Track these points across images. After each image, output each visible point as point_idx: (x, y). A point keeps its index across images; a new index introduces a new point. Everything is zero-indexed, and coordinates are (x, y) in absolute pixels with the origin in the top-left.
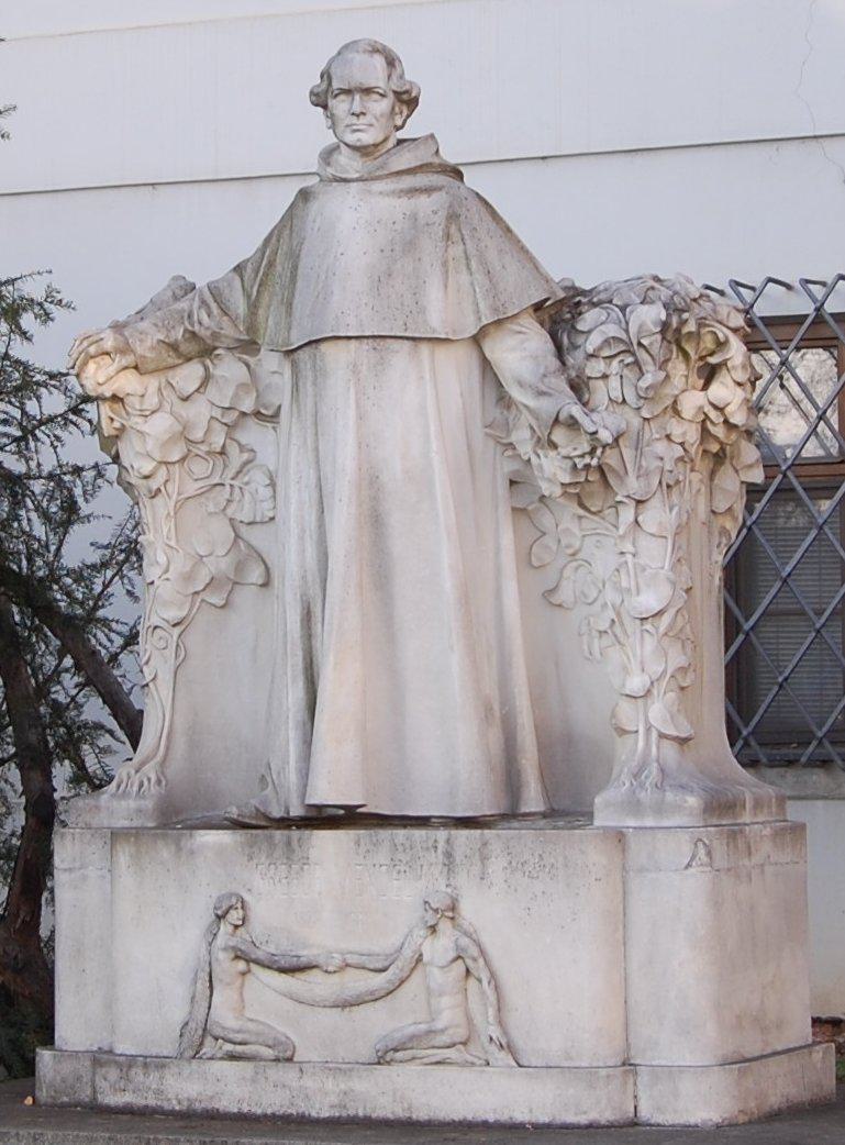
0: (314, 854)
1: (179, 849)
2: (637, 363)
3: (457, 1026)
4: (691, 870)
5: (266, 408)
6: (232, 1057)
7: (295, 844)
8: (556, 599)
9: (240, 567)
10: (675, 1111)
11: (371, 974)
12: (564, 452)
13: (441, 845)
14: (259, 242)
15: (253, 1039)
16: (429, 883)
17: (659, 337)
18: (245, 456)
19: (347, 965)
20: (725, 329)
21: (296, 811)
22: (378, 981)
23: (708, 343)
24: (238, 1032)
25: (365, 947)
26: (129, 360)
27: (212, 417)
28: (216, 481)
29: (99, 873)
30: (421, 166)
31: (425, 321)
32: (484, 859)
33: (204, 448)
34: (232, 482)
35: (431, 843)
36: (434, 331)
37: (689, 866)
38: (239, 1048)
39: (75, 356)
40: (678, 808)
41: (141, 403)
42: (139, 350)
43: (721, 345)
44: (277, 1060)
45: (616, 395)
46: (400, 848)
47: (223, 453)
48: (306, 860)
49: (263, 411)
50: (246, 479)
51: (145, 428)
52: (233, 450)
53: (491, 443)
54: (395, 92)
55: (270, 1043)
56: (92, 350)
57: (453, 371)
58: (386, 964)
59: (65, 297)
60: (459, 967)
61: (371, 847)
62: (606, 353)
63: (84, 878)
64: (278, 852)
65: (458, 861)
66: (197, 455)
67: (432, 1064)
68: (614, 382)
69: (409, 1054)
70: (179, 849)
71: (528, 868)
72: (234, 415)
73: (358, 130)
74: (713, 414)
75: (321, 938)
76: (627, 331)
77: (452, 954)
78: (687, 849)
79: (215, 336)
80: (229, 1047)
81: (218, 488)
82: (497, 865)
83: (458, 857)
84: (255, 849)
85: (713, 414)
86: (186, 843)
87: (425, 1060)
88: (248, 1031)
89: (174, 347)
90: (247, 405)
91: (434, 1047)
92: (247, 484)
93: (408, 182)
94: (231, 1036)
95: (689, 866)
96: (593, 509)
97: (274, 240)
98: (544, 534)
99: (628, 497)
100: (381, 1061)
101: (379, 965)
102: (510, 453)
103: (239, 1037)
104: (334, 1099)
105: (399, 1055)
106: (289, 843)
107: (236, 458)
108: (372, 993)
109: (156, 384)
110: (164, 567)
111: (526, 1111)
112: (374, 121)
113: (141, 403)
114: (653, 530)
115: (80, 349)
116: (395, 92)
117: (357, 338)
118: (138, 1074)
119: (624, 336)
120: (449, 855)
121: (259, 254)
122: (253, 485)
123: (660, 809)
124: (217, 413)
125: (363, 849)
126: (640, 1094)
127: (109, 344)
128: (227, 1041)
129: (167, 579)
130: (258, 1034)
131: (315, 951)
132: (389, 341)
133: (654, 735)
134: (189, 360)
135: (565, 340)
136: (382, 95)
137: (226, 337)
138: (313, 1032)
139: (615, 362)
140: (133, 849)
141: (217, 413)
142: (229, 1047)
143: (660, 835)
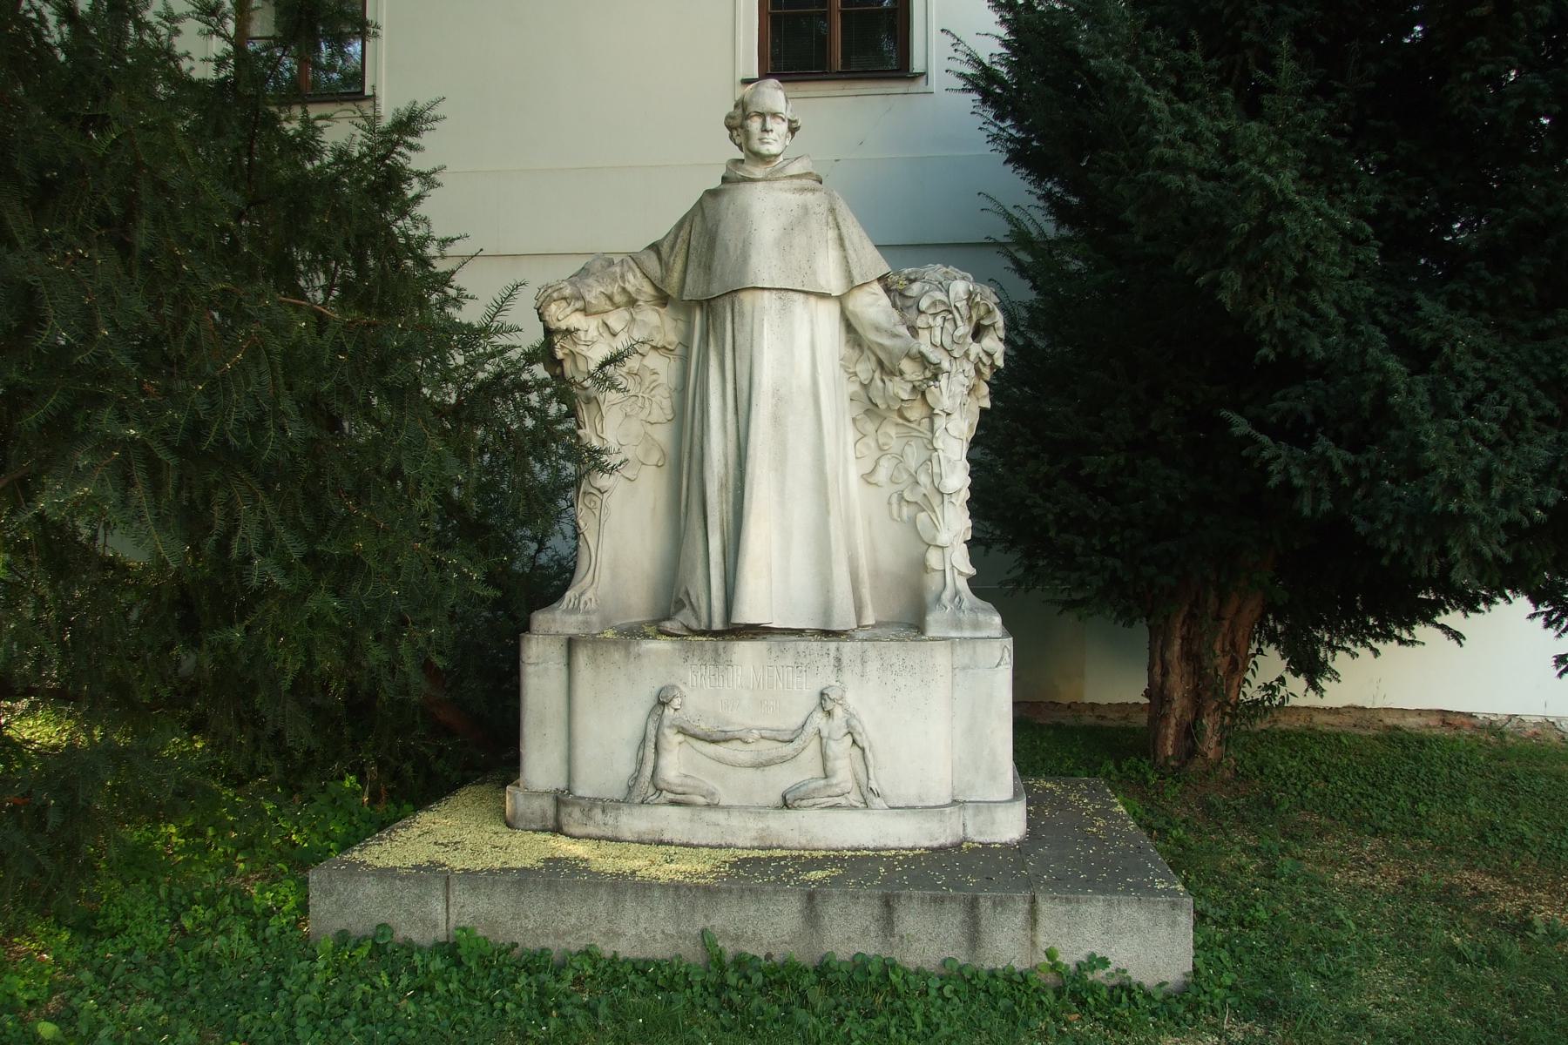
0: (735, 658)
1: (628, 653)
2: (954, 320)
3: (846, 782)
4: (1000, 667)
7: (721, 651)
10: (992, 834)
11: (780, 744)
13: (833, 653)
14: (675, 222)
15: (691, 790)
16: (823, 677)
17: (965, 302)
19: (762, 738)
21: (718, 625)
22: (788, 749)
23: (982, 310)
24: (679, 786)
25: (776, 724)
26: (579, 304)
29: (557, 666)
30: (806, 174)
31: (816, 281)
32: (863, 662)
35: (825, 651)
37: (999, 664)
38: (679, 797)
39: (541, 300)
40: (989, 625)
41: (585, 336)
42: (589, 297)
43: (989, 312)
44: (708, 805)
46: (803, 655)
48: (729, 664)
51: (588, 354)
53: (842, 371)
54: (789, 120)
55: (704, 793)
56: (555, 295)
57: (826, 317)
58: (792, 737)
59: (469, 292)
60: (849, 739)
61: (779, 653)
62: (932, 311)
63: (546, 670)
64: (707, 657)
65: (844, 664)
67: (826, 807)
68: (937, 332)
69: (811, 802)
70: (628, 653)
71: (895, 668)
74: (985, 359)
75: (739, 718)
76: (948, 296)
77: (846, 731)
78: (998, 654)
80: (671, 796)
81: (634, 399)
82: (873, 666)
83: (845, 661)
84: (690, 654)
85: (985, 359)
86: (634, 649)
88: (688, 786)
89: (610, 298)
91: (829, 796)
93: (797, 183)
94: (674, 788)
95: (999, 664)
96: (912, 419)
97: (687, 226)
98: (865, 436)
99: (943, 411)
100: (785, 804)
101: (787, 738)
102: (854, 378)
103: (680, 790)
104: (753, 834)
105: (804, 803)
106: (716, 651)
108: (781, 758)
109: (596, 323)
111: (896, 839)
113: (585, 336)
114: (956, 434)
115: (546, 294)
116: (789, 120)
117: (769, 289)
118: (597, 814)
119: (946, 299)
120: (838, 660)
121: (671, 237)
122: (658, 397)
123: (976, 625)
125: (774, 655)
126: (967, 822)
127: (568, 292)
128: (672, 792)
130: (696, 787)
131: (737, 728)
132: (791, 293)
133: (956, 571)
134: (618, 307)
136: (784, 120)
137: (645, 292)
138: (733, 785)
139: (939, 320)
140: (590, 652)
142: (671, 796)
143: (979, 643)
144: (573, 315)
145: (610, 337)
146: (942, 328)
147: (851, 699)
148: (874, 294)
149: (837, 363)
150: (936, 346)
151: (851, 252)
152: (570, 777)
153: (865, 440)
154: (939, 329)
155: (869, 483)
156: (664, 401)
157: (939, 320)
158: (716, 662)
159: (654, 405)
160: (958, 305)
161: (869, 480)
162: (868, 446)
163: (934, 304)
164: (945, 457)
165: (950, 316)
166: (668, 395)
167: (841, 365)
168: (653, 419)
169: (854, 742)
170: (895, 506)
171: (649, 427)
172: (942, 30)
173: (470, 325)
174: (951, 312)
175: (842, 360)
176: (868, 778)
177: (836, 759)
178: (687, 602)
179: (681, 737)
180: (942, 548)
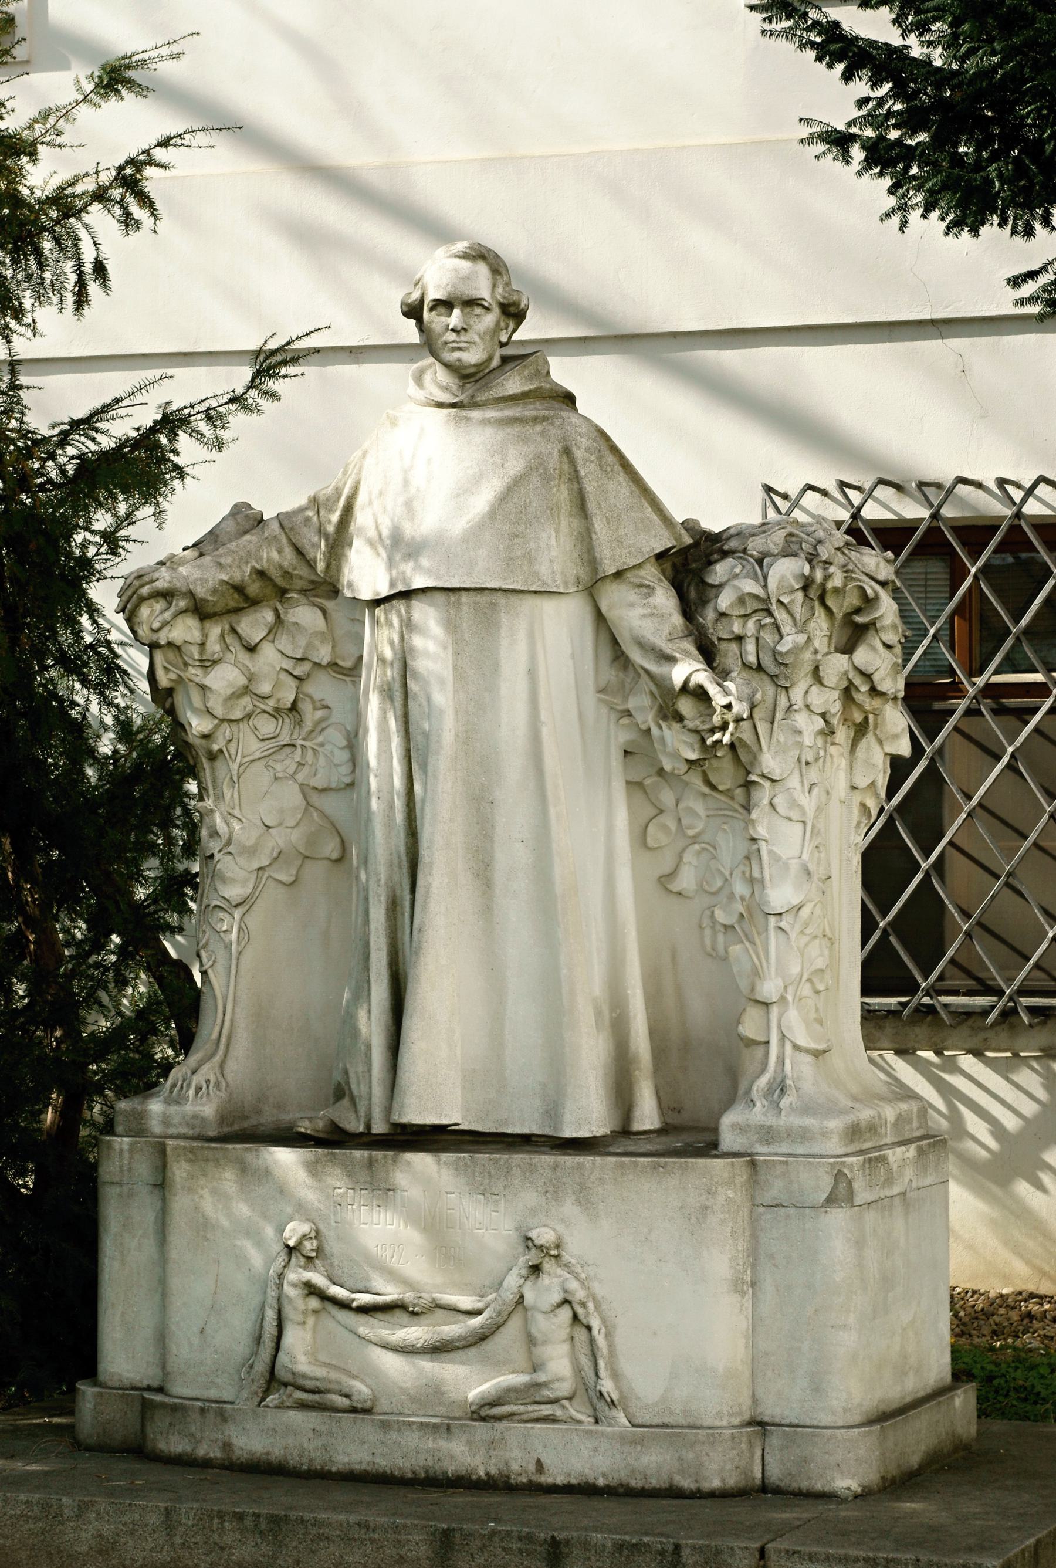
2: (777, 627)
5: (344, 660)
6: (303, 1406)
8: (675, 887)
9: (312, 840)
12: (690, 724)
18: (319, 714)
20: (873, 584)
21: (379, 1128)
27: (281, 669)
28: (285, 739)
33: (272, 703)
34: (304, 743)
36: (544, 584)
45: (752, 659)
47: (294, 707)
49: (341, 663)
50: (320, 739)
51: (207, 682)
52: (306, 707)
53: (604, 711)
60: (565, 1313)
66: (264, 711)
68: (750, 647)
72: (306, 667)
73: (459, 349)
74: (857, 681)
76: (765, 586)
79: (287, 574)
80: (299, 1395)
81: (288, 750)
85: (857, 681)
87: (525, 1417)
90: (324, 654)
92: (322, 745)
96: (721, 788)
98: (661, 811)
102: (625, 721)
103: (309, 1384)
107: (310, 715)
110: (224, 841)
112: (476, 339)
122: (328, 747)
124: (288, 664)
129: (230, 853)
135: (693, 594)
139: (751, 624)
141: (288, 664)
144: (180, 620)
145: (243, 656)
146: (757, 639)
147: (572, 1251)
148: (641, 586)
149: (591, 697)
150: (751, 668)
151: (598, 524)
152: (163, 1366)
153: (661, 819)
154: (753, 640)
155: (667, 889)
156: (337, 752)
157: (751, 624)
158: (953, 1436)
159: (322, 761)
160: (785, 600)
161: (668, 886)
162: (664, 828)
163: (741, 600)
164: (770, 852)
165: (768, 620)
166: (344, 743)
167: (600, 700)
168: (319, 782)
169: (575, 1317)
170: (708, 932)
171: (315, 799)
172: (801, 120)
173: (156, 422)
174: (770, 613)
175: (599, 692)
176: (597, 1375)
177: (545, 1343)
178: (347, 1092)
179: (314, 1303)
180: (766, 1005)
